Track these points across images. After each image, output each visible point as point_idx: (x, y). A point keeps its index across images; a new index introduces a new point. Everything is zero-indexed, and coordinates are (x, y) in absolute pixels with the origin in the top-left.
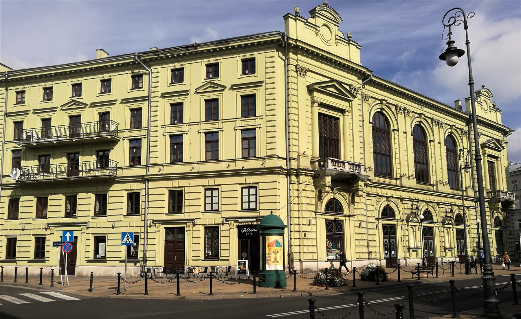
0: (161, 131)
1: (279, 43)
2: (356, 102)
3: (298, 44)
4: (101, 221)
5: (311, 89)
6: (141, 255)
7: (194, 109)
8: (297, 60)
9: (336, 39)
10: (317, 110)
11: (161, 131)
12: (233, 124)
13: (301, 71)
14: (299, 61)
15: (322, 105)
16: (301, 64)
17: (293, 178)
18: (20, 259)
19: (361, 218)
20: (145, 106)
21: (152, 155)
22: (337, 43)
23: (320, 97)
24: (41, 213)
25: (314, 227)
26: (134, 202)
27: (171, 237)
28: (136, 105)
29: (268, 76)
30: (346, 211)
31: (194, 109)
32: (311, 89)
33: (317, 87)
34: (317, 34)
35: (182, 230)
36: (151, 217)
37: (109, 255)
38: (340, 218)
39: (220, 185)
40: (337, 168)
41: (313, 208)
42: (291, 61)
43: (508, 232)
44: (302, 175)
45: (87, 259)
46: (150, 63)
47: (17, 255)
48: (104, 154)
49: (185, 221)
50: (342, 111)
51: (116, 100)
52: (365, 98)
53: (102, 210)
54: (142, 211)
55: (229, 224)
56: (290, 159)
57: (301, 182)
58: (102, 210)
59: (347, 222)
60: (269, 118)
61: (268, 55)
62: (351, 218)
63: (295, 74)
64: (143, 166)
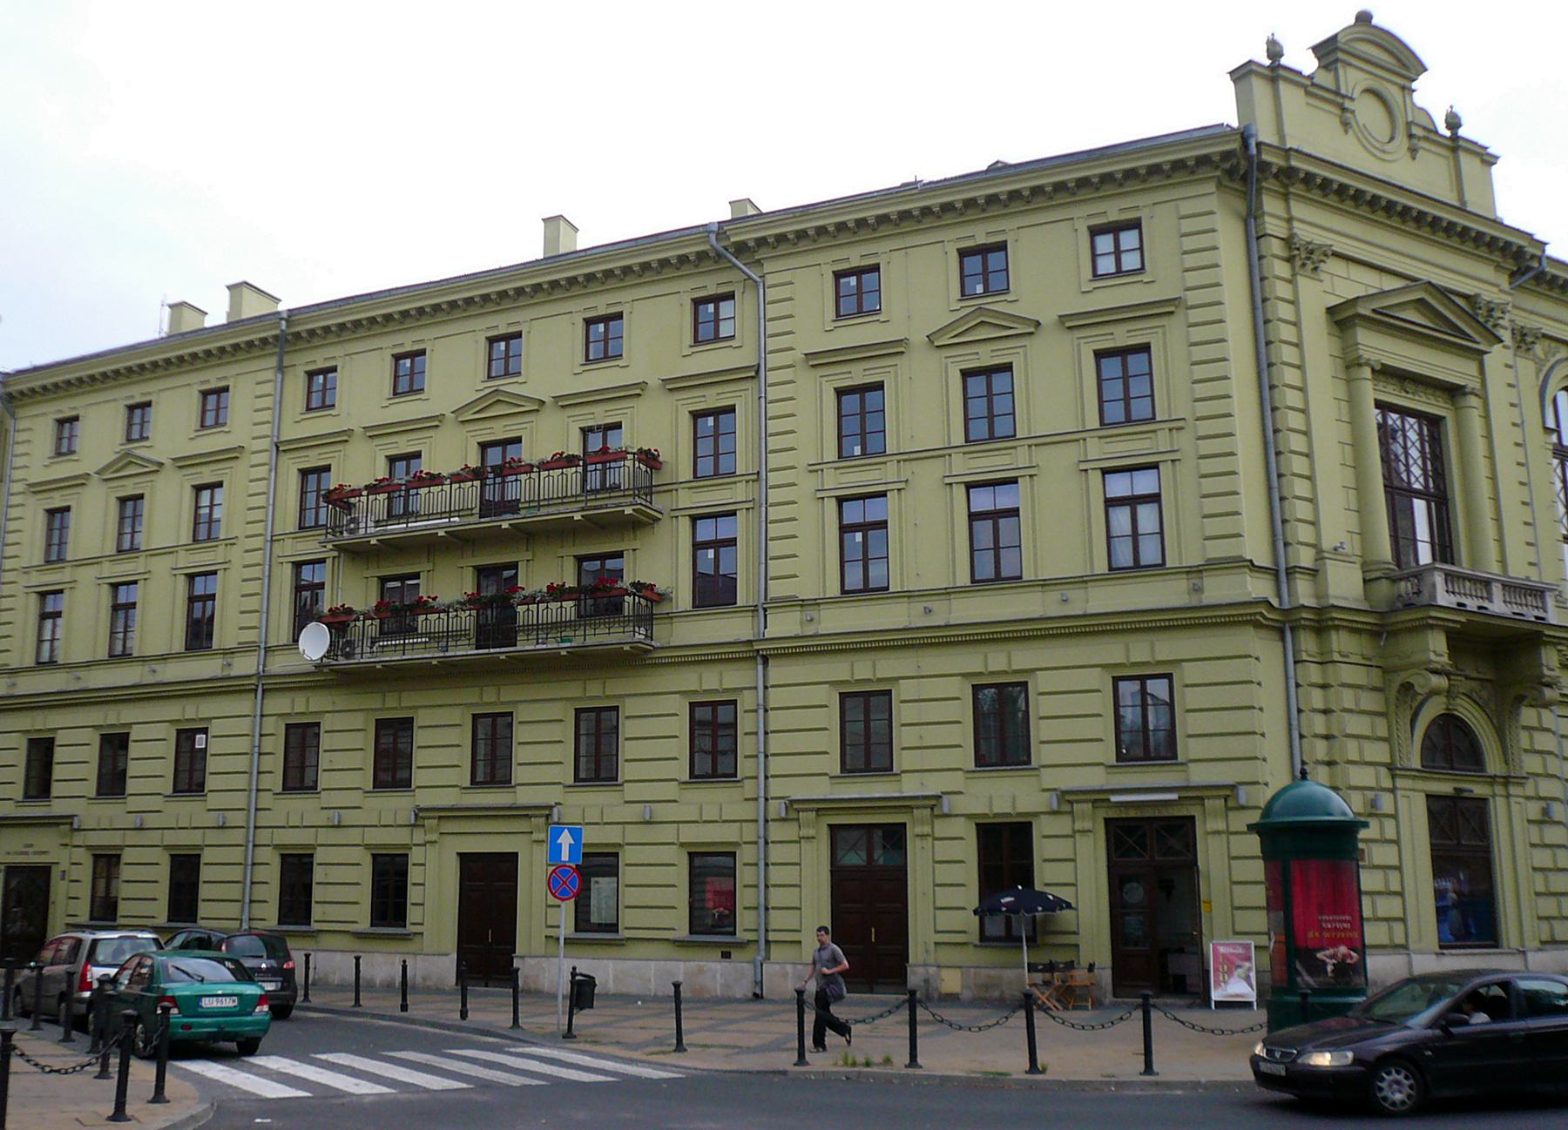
0: (809, 483)
1: (1227, 165)
2: (1497, 357)
3: (1294, 163)
4: (594, 801)
5: (1342, 318)
6: (745, 920)
7: (923, 406)
8: (1290, 220)
9: (1411, 136)
10: (1370, 391)
11: (809, 483)
12: (1071, 453)
13: (1304, 257)
14: (1296, 224)
15: (1385, 373)
16: (1304, 233)
17: (1308, 643)
18: (325, 926)
19: (1548, 788)
20: (741, 398)
21: (775, 568)
22: (1413, 151)
23: (1376, 346)
24: (392, 769)
25: (1389, 825)
26: (714, 742)
27: (855, 859)
28: (712, 398)
29: (1193, 279)
30: (1494, 765)
31: (923, 406)
32: (1342, 318)
33: (1364, 310)
34: (1346, 125)
35: (895, 836)
36: (777, 788)
37: (628, 919)
38: (1479, 790)
39: (1033, 671)
40: (1463, 600)
41: (1380, 753)
42: (1273, 226)
43: (1534, 810)
44: (1337, 628)
45: (71, 920)
46: (762, 253)
47: (317, 912)
48: (603, 565)
49: (906, 804)
50: (1453, 392)
51: (643, 385)
52: (1524, 340)
53: (598, 760)
54: (745, 767)
55: (1071, 813)
56: (1291, 571)
57: (1336, 657)
58: (598, 760)
59: (1500, 802)
60: (1206, 428)
61: (1187, 207)
62: (1513, 790)
63: (1282, 269)
64: (744, 610)
